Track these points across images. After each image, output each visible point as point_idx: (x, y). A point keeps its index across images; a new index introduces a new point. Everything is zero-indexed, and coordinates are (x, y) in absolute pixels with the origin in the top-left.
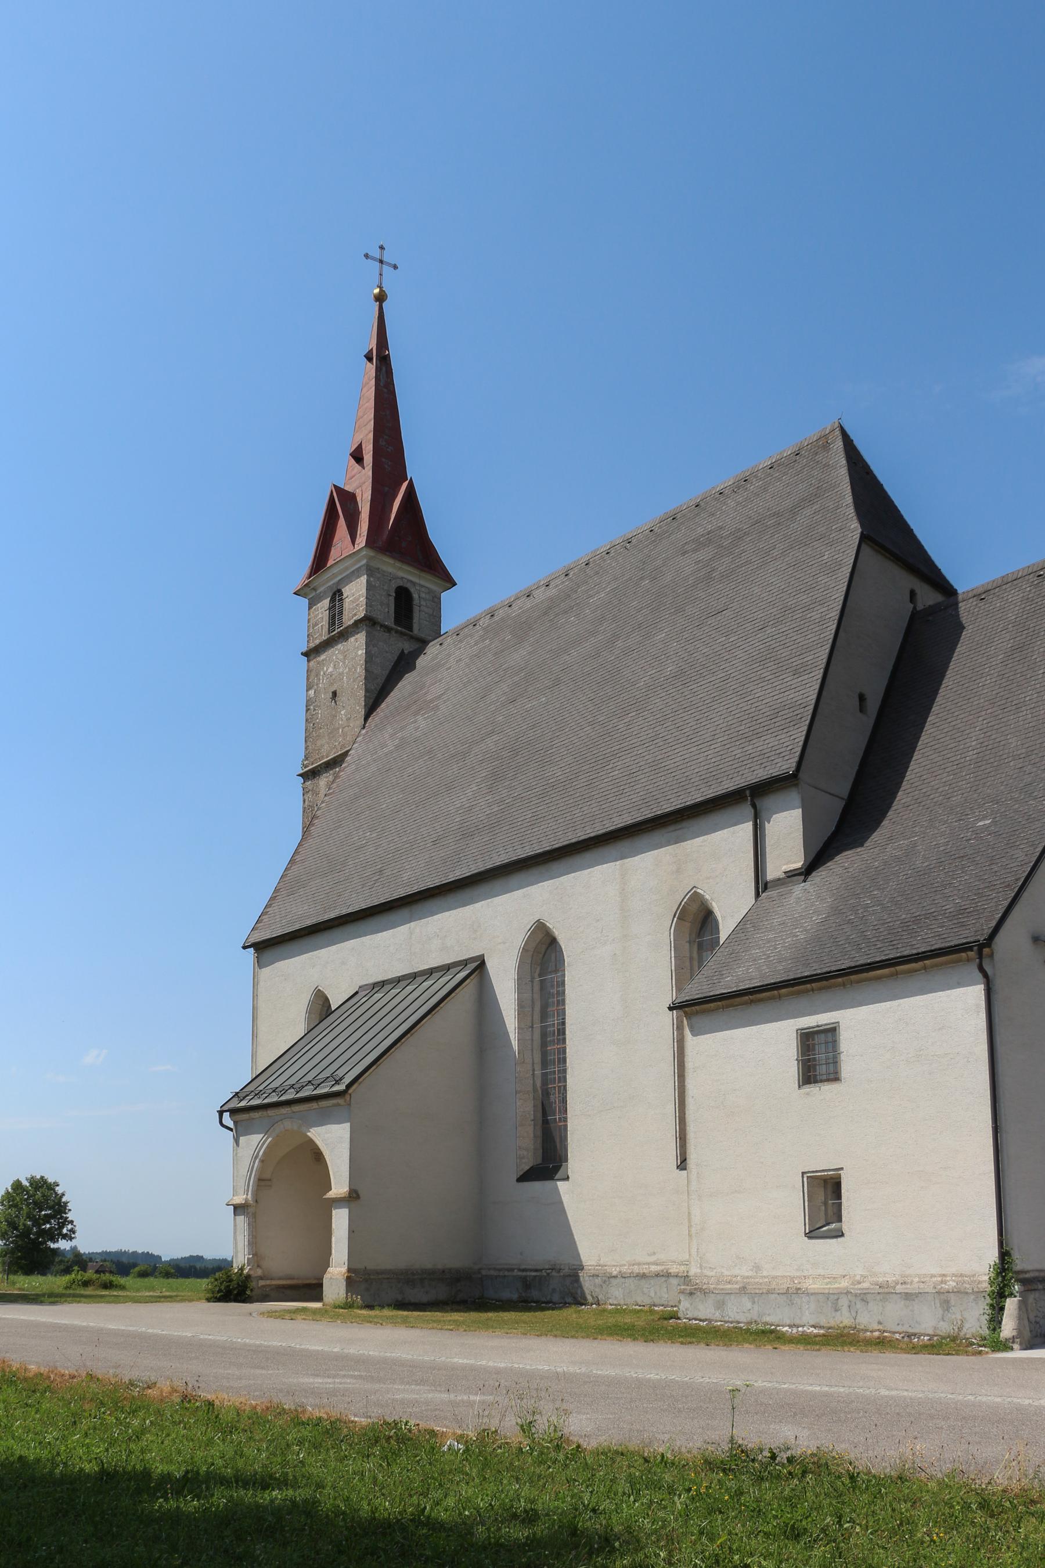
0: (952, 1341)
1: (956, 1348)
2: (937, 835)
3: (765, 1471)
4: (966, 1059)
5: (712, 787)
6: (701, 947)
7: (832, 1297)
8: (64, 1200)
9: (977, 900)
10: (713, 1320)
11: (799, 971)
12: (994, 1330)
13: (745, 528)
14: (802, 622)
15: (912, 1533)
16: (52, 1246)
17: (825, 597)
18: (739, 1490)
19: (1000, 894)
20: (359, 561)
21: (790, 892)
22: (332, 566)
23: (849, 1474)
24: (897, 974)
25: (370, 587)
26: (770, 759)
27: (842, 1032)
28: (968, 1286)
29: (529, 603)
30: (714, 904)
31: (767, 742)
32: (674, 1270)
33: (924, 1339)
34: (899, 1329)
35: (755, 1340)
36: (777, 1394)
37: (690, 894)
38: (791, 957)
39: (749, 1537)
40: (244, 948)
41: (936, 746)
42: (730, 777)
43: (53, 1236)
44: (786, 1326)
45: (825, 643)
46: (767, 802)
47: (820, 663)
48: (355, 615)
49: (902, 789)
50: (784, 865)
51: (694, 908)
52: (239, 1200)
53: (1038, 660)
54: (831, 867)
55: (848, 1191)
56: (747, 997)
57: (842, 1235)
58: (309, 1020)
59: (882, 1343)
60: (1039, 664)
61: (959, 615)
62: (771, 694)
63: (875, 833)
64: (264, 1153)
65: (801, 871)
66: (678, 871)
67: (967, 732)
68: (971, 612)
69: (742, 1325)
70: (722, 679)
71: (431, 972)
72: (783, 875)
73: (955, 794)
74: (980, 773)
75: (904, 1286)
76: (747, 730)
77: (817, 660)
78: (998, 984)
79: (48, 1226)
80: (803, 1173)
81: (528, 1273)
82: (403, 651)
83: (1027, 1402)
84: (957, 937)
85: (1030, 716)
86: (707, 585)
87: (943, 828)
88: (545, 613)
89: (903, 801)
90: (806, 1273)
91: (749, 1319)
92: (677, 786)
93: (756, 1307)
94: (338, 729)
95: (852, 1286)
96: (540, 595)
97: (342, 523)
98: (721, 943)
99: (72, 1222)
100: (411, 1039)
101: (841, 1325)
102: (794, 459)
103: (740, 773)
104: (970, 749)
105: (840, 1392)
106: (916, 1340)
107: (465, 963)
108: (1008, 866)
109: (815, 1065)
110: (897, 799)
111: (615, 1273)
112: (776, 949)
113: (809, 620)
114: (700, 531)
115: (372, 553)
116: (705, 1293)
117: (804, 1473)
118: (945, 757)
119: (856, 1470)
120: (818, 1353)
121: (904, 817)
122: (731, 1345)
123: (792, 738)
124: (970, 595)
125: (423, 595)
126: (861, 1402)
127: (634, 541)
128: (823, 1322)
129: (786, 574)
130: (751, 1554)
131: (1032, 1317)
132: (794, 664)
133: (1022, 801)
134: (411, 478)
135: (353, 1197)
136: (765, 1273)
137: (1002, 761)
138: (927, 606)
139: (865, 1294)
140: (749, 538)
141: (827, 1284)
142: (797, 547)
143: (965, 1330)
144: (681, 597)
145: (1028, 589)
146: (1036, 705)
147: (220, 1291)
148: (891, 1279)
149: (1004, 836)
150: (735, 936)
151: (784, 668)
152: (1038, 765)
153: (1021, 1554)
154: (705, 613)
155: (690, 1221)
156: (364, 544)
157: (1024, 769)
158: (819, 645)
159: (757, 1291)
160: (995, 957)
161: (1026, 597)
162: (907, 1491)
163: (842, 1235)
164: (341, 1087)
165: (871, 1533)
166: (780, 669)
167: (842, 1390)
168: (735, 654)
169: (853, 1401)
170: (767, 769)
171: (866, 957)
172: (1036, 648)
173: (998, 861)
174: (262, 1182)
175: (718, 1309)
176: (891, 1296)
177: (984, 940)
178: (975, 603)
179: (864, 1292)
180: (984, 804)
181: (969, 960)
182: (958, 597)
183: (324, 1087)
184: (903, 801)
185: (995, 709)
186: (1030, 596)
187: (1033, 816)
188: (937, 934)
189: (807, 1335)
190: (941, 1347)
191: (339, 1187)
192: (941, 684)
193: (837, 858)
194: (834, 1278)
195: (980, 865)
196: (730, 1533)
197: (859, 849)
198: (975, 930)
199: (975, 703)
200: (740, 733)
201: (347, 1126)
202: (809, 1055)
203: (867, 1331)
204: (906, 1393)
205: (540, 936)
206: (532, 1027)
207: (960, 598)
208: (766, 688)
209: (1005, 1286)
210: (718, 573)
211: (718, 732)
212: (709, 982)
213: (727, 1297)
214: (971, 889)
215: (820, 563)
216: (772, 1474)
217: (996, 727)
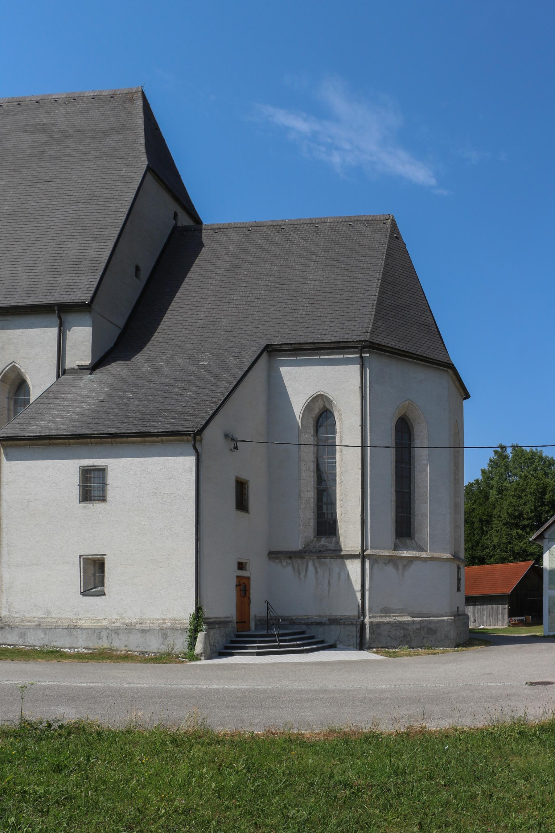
0: (167, 655)
1: (170, 660)
2: (176, 364)
3: (43, 735)
4: (183, 498)
5: (31, 298)
6: (16, 402)
7: (97, 631)
9: (195, 407)
10: (17, 645)
11: (83, 430)
12: (191, 649)
13: (70, 131)
14: (103, 208)
15: (131, 760)
17: (120, 197)
18: (25, 747)
19: (209, 407)
23: (97, 732)
24: (145, 442)
26: (74, 290)
27: (109, 472)
28: (178, 626)
31: (72, 278)
33: (151, 655)
34: (137, 649)
35: (46, 657)
36: (58, 689)
37: (10, 366)
38: (79, 420)
39: (28, 775)
41: (180, 311)
42: (45, 294)
44: (67, 648)
45: (117, 226)
46: (69, 318)
47: (112, 238)
49: (157, 331)
50: (78, 361)
51: (13, 376)
53: (243, 278)
54: (109, 369)
55: (108, 569)
56: (47, 441)
57: (104, 594)
59: (127, 658)
60: (243, 280)
61: (201, 237)
62: (78, 248)
63: (138, 354)
65: (89, 367)
67: (199, 308)
68: (209, 238)
69: (37, 648)
70: (44, 228)
72: (76, 367)
73: (189, 342)
74: (204, 334)
75: (141, 625)
76: (59, 267)
77: (110, 235)
78: (204, 458)
80: (80, 556)
83: (205, 687)
84: (182, 427)
85: (235, 309)
86: (39, 160)
87: (180, 361)
89: (157, 339)
91: (42, 644)
92: (5, 290)
93: (47, 637)
95: (109, 625)
98: (31, 402)
101: (102, 648)
103: (52, 294)
104: (200, 318)
105: (99, 686)
106: (147, 655)
108: (215, 392)
109: (91, 490)
110: (154, 337)
112: (69, 413)
113: (108, 208)
114: (37, 120)
116: (12, 628)
117: (69, 734)
118: (185, 319)
119: (102, 730)
120: (87, 664)
121: (157, 349)
122: (29, 660)
123: (90, 280)
124: (209, 227)
126: (111, 692)
128: (91, 646)
129: (95, 173)
130: (29, 784)
131: (212, 642)
132: (95, 233)
133: (226, 356)
136: (53, 616)
137: (217, 331)
138: (183, 225)
139: (117, 629)
140: (73, 140)
141: (94, 623)
142: (105, 158)
143: (175, 650)
144: (18, 161)
145: (242, 236)
146: (239, 303)
148: (133, 621)
149: (214, 373)
150: (41, 400)
151: (88, 234)
152: (237, 338)
153: (190, 763)
154: (36, 179)
157: (229, 338)
158: (113, 227)
159: (48, 627)
160: (203, 442)
161: (240, 240)
162: (131, 738)
163: (104, 594)
165: (107, 763)
166: (85, 233)
167: (100, 685)
168: (55, 214)
169: (106, 691)
170: (71, 296)
171: (126, 429)
172: (242, 271)
173: (209, 387)
175: (21, 638)
176: (133, 630)
177: (198, 431)
178: (211, 233)
179: (117, 628)
180: (205, 352)
182: (202, 226)
184: (157, 339)
185: (216, 299)
186: (243, 240)
187: (231, 366)
188: (170, 422)
189: (80, 653)
190: (161, 659)
192: (187, 275)
193: (113, 364)
194: (99, 620)
195: (199, 388)
196: (16, 774)
197: (127, 362)
199: (205, 292)
200: (54, 267)
202: (87, 484)
203: (118, 650)
204: (138, 685)
207: (204, 227)
208: (74, 243)
209: (198, 626)
210: (48, 154)
211: (38, 262)
212: (20, 427)
213: (28, 630)
214: (193, 400)
215: (120, 174)
216: (47, 736)
217: (215, 310)
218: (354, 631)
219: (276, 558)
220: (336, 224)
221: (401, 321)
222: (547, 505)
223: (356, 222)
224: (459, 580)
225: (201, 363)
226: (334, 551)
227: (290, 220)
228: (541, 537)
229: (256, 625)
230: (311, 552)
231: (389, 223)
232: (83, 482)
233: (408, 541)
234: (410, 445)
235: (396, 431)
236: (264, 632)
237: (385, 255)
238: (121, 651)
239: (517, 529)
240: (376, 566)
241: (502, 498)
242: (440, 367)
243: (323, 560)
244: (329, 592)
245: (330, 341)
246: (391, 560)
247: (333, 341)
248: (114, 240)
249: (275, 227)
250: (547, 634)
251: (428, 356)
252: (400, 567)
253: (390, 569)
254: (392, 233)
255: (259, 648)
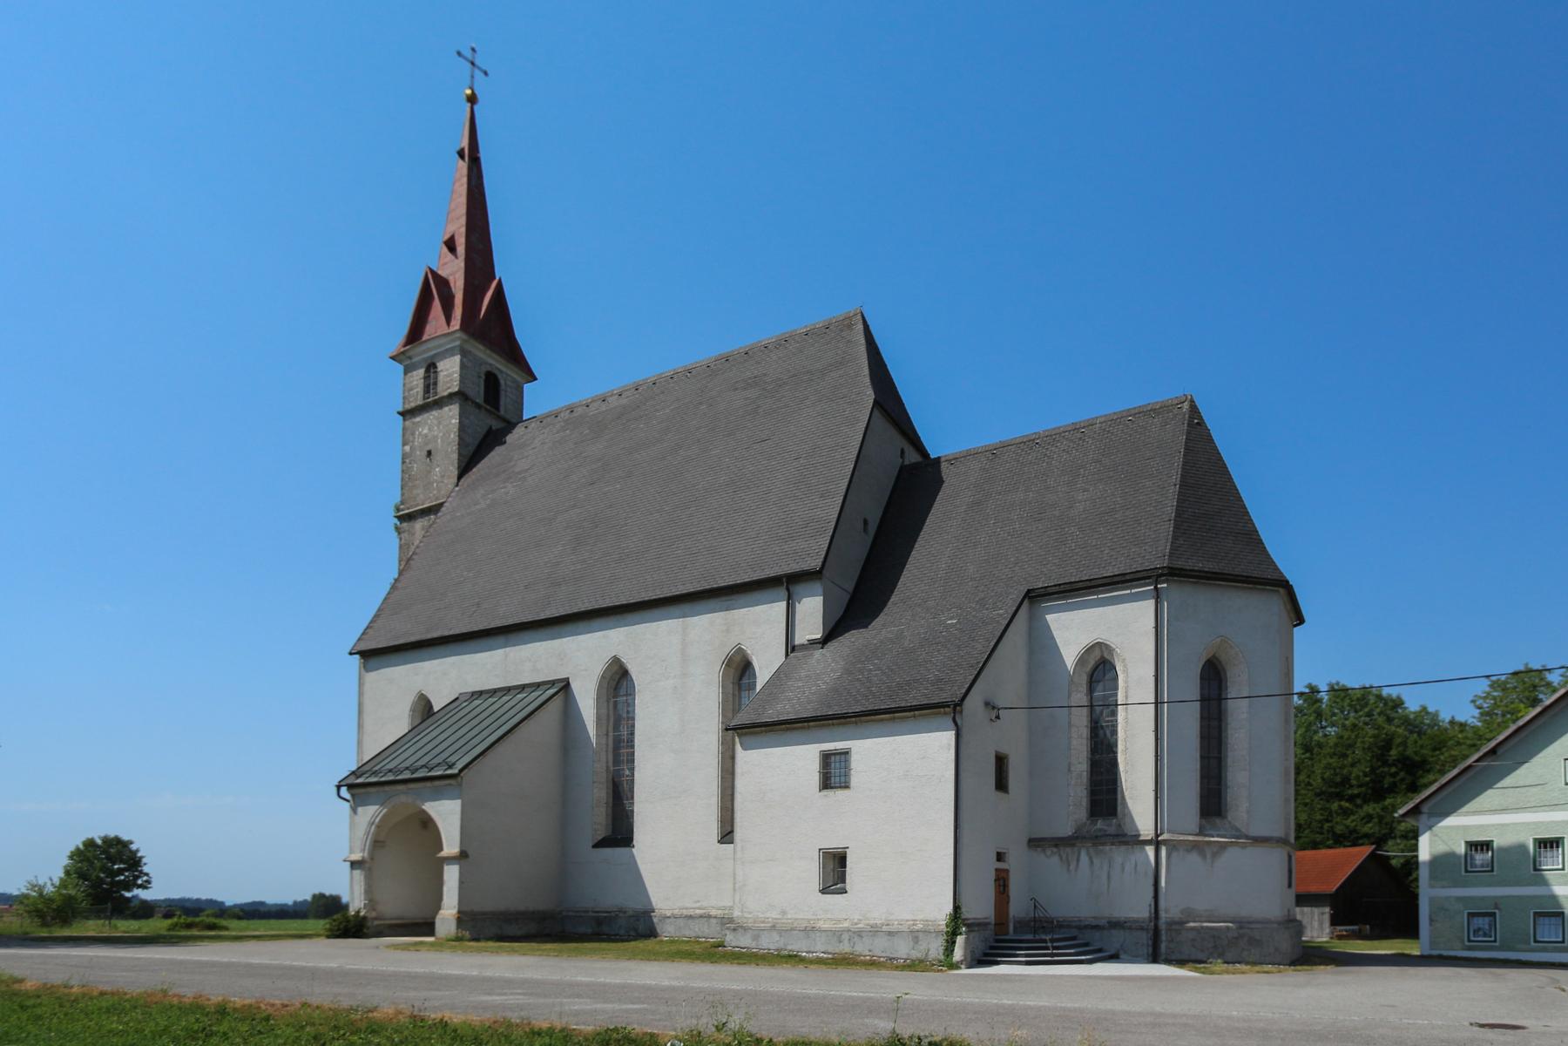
6: (740, 689)
8: (139, 855)
12: (948, 956)
16: (128, 895)
20: (453, 341)
21: (812, 655)
22: (425, 341)
24: (894, 718)
25: (463, 366)
29: (604, 407)
30: (753, 657)
32: (713, 913)
34: (884, 955)
40: (351, 654)
43: (128, 886)
46: (798, 589)
48: (449, 388)
51: (738, 658)
52: (357, 856)
58: (413, 717)
59: (873, 964)
64: (380, 820)
66: (728, 631)
71: (523, 687)
72: (806, 642)
78: (964, 731)
79: (122, 878)
80: (820, 850)
81: (600, 914)
82: (491, 427)
88: (618, 418)
90: (819, 917)
94: (433, 483)
96: (613, 402)
97: (437, 305)
99: (147, 874)
100: (511, 737)
102: (824, 331)
107: (553, 683)
111: (668, 915)
115: (465, 337)
116: (746, 929)
125: (508, 383)
127: (694, 372)
134: (500, 280)
135: (463, 855)
136: (789, 917)
141: (834, 924)
147: (338, 930)
155: (735, 879)
156: (458, 327)
163: (846, 892)
164: (455, 771)
174: (377, 844)
181: (945, 713)
183: (438, 771)
191: (451, 847)
198: (949, 694)
201: (459, 802)
205: (616, 668)
206: (607, 735)
213: (761, 932)
218: (1145, 938)
219: (1038, 846)
220: (1109, 423)
221: (1210, 535)
222: (1394, 765)
223: (1137, 416)
224: (1290, 871)
225: (949, 622)
226: (1117, 836)
227: (1046, 431)
228: (1416, 811)
229: (1015, 928)
230: (1084, 838)
231: (1186, 406)
232: (824, 768)
233: (1218, 821)
234: (1220, 695)
235: (1202, 678)
236: (1030, 937)
237: (1182, 450)
238: (865, 956)
239: (1341, 800)
240: (1174, 854)
241: (1311, 759)
242: (1268, 587)
243: (1101, 847)
244: (1109, 886)
245: (1111, 574)
246: (1195, 846)
247: (1116, 573)
248: (843, 494)
249: (1027, 443)
250: (1426, 953)
251: (1249, 575)
252: (1209, 856)
253: (1194, 858)
254: (1191, 418)
255: (1027, 956)
